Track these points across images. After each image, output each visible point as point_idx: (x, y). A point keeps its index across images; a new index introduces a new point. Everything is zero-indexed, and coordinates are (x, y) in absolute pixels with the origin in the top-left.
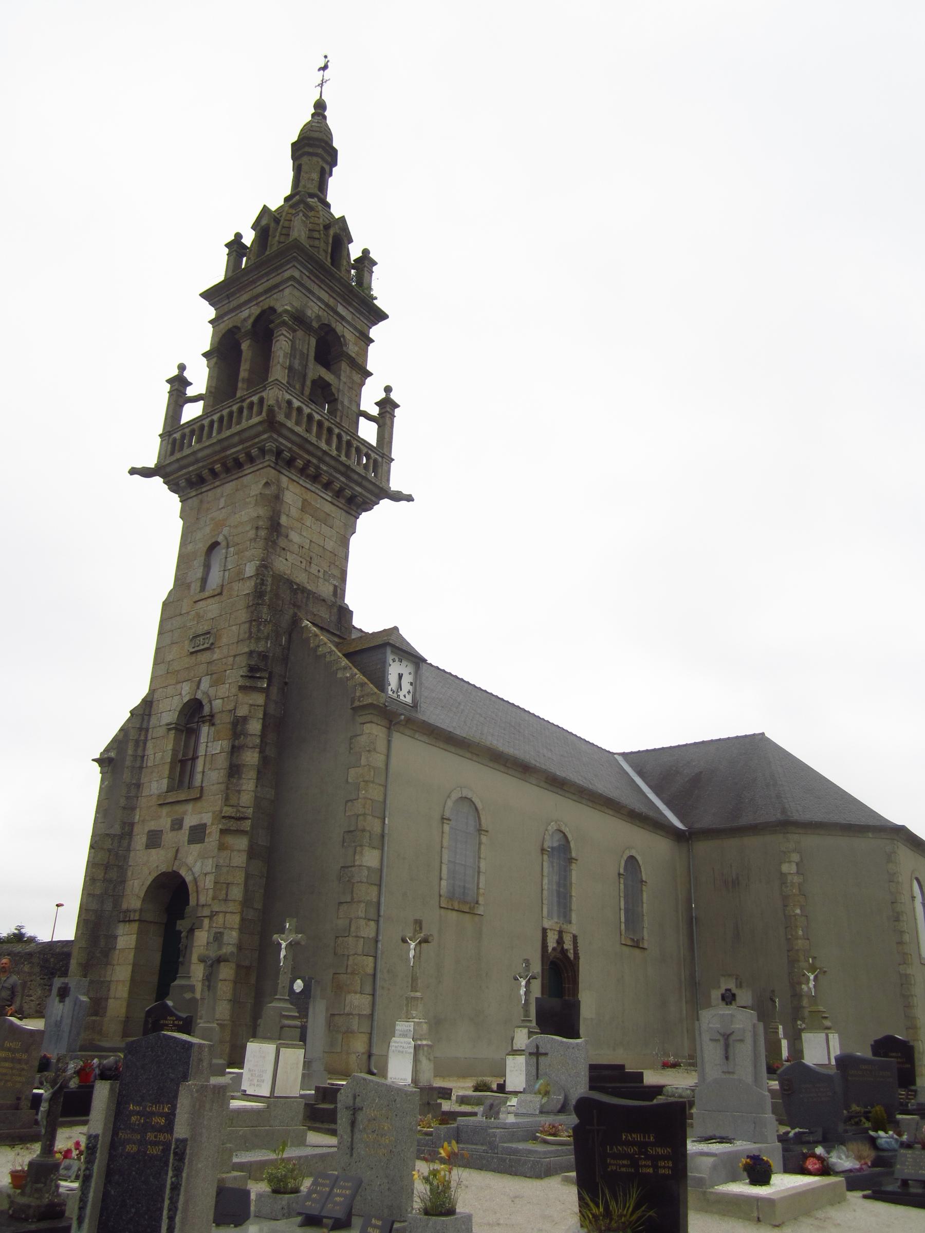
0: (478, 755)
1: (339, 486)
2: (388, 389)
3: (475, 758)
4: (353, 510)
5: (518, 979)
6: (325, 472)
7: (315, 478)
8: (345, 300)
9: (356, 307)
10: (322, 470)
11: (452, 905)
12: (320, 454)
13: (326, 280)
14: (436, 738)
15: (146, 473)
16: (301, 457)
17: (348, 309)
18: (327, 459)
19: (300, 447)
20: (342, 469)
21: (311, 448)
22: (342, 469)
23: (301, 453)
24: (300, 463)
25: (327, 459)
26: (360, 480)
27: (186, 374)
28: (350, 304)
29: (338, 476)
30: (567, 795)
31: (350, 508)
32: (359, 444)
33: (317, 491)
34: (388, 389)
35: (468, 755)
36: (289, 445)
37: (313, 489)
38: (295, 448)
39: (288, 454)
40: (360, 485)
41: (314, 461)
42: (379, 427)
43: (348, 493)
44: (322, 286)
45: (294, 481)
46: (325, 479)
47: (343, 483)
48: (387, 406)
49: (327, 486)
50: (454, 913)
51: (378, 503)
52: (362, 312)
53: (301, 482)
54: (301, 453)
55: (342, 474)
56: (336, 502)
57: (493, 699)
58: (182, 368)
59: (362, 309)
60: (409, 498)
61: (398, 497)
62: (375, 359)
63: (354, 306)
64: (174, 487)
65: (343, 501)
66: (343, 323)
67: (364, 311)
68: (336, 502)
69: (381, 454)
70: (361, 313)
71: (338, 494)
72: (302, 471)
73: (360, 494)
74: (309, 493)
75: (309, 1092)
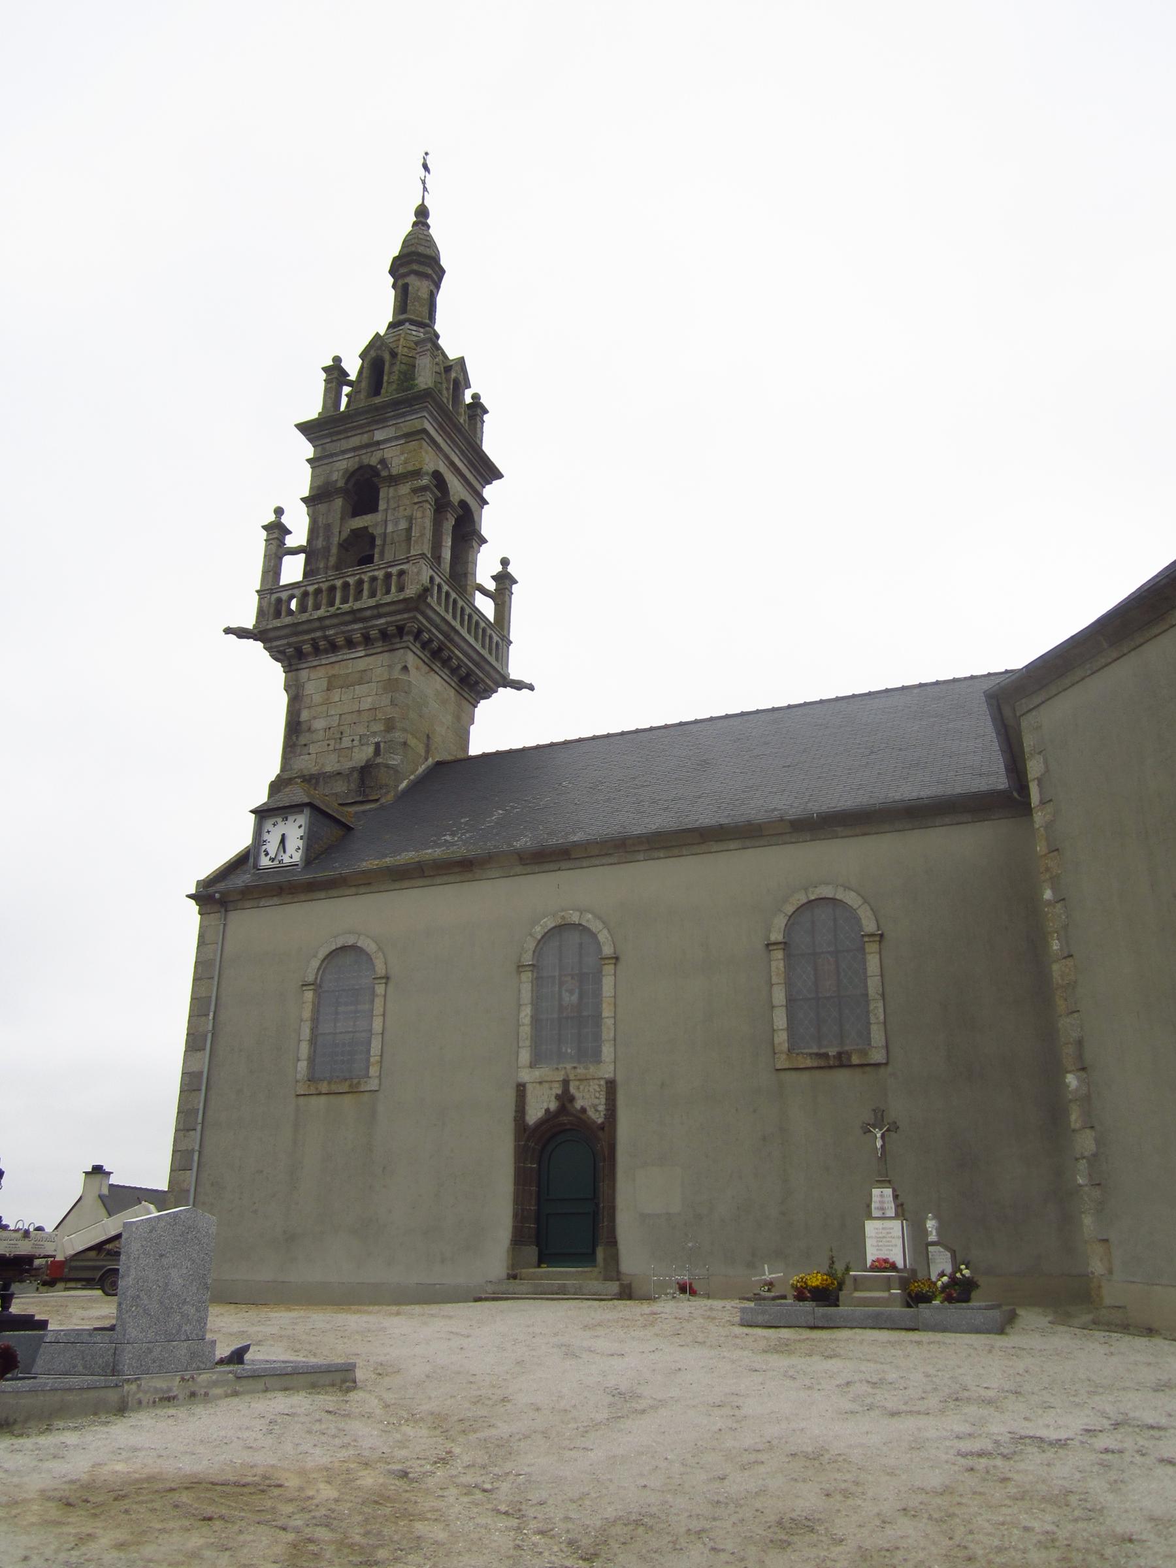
0: (369, 884)
1: (359, 635)
2: (505, 562)
3: (362, 890)
4: (395, 643)
5: (871, 1131)
6: (335, 635)
7: (333, 648)
8: (377, 422)
9: (393, 416)
10: (331, 635)
11: (317, 1089)
12: (317, 624)
13: (347, 426)
14: (293, 894)
15: (241, 633)
16: (304, 642)
17: (388, 426)
18: (327, 622)
19: (296, 634)
20: (348, 618)
21: (305, 627)
22: (348, 618)
23: (301, 638)
24: (307, 648)
25: (327, 622)
26: (375, 612)
27: (510, 569)
28: (386, 420)
29: (349, 628)
30: (585, 864)
31: (392, 644)
32: (371, 574)
33: (345, 657)
34: (505, 562)
35: (353, 890)
36: (284, 642)
37: (340, 658)
38: (293, 640)
39: (291, 650)
40: (380, 616)
41: (318, 634)
42: (496, 604)
43: (374, 633)
44: (349, 434)
45: (315, 667)
46: (340, 640)
47: (361, 629)
48: (504, 580)
49: (350, 644)
50: (323, 1099)
51: (497, 692)
52: (404, 413)
53: (324, 662)
54: (301, 638)
55: (354, 621)
56: (372, 651)
57: (693, 728)
58: (279, 512)
59: (401, 411)
60: (531, 688)
61: (518, 685)
62: (489, 522)
63: (390, 417)
64: (277, 654)
65: (380, 643)
66: (381, 447)
67: (404, 410)
68: (372, 651)
69: (405, 561)
70: (403, 415)
71: (367, 640)
72: (317, 651)
73: (387, 623)
74: (337, 666)
75: (779, 1275)
